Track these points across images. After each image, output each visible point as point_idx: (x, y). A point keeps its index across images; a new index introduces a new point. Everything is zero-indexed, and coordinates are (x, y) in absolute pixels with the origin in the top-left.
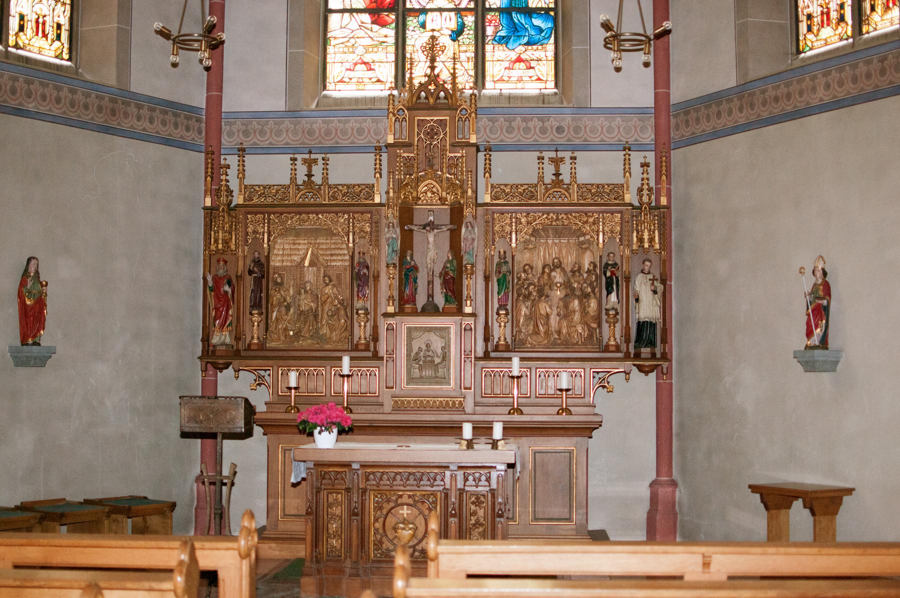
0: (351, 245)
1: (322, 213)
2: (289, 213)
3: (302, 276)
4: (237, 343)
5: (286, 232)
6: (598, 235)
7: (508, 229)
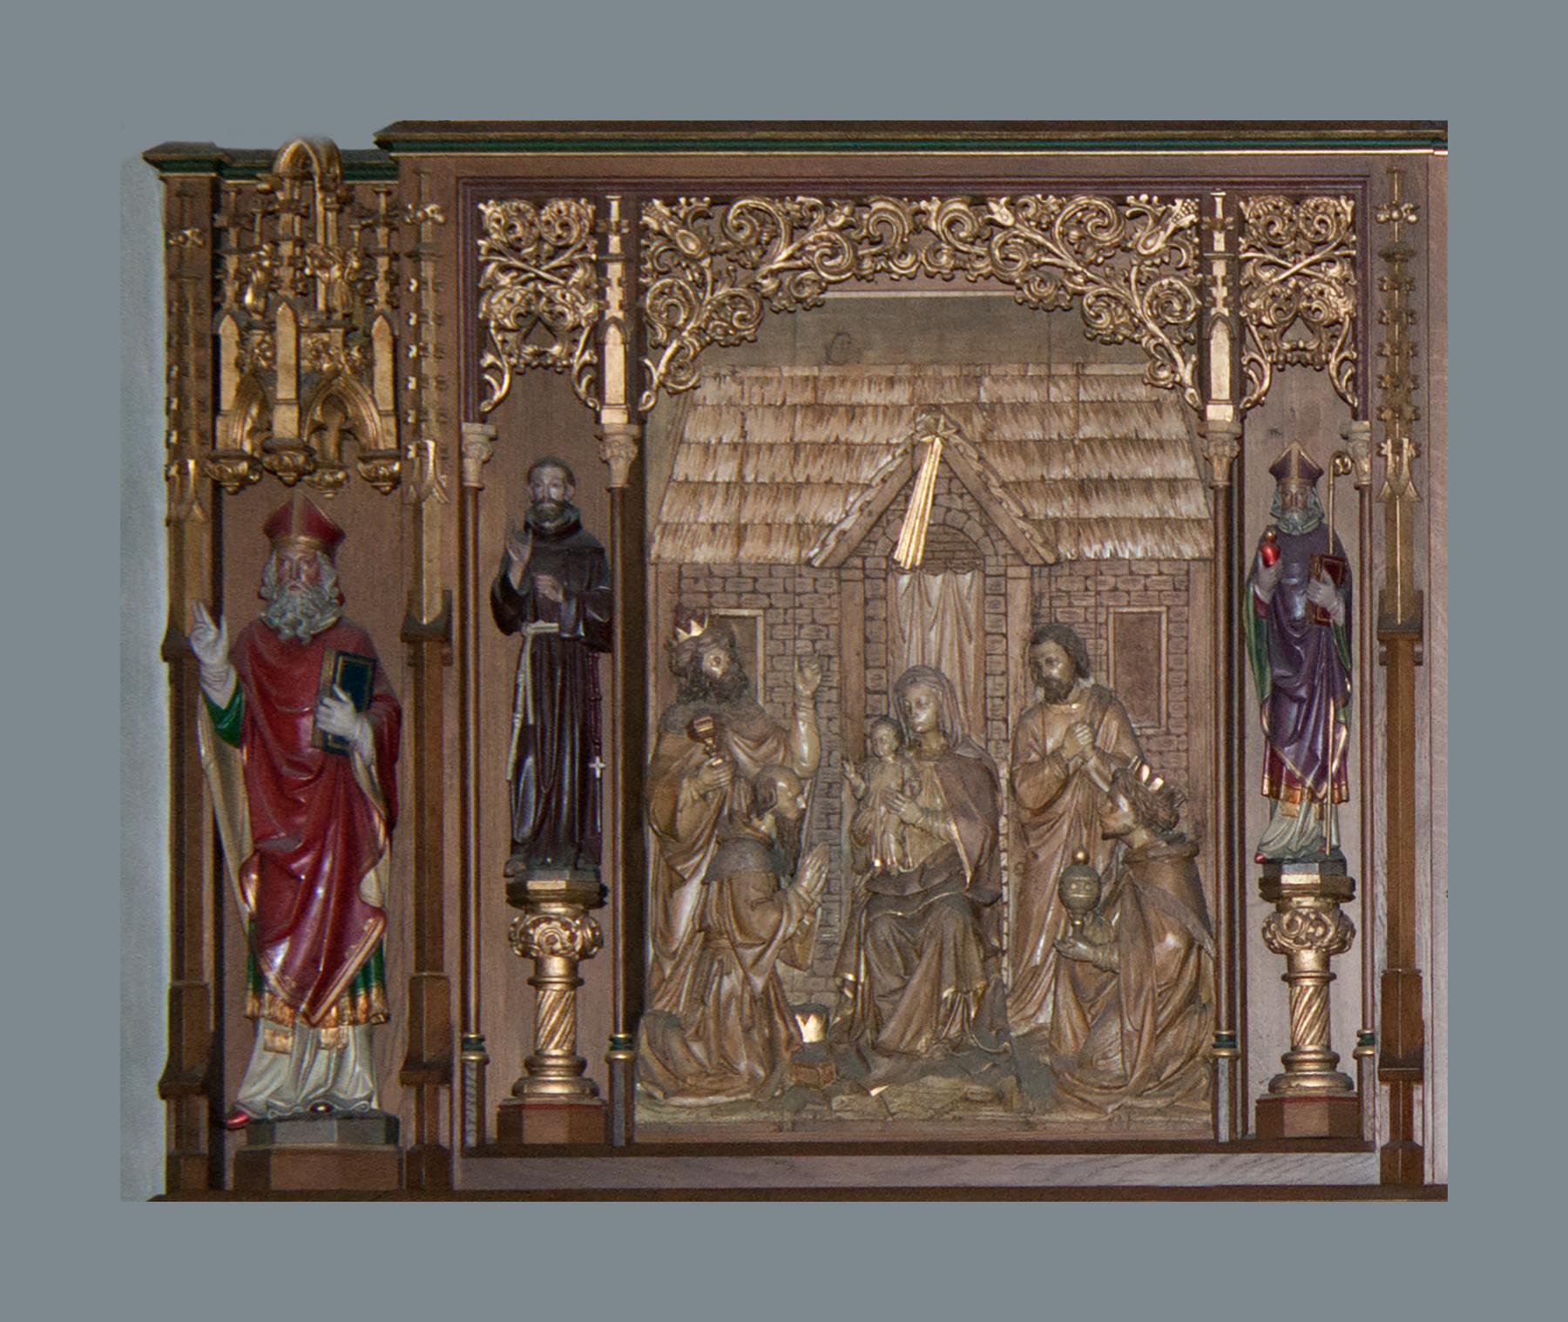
0: (1220, 414)
1: (1016, 187)
2: (781, 189)
3: (877, 639)
4: (426, 1108)
5: (761, 324)
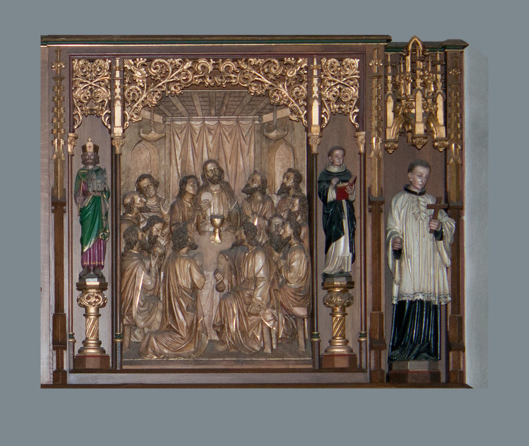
6: (309, 108)
7: (103, 93)
